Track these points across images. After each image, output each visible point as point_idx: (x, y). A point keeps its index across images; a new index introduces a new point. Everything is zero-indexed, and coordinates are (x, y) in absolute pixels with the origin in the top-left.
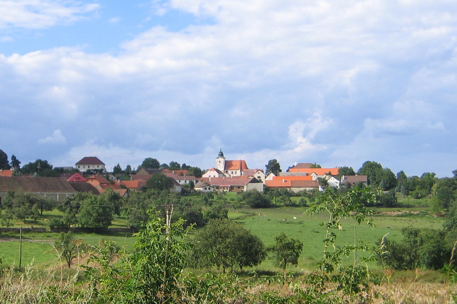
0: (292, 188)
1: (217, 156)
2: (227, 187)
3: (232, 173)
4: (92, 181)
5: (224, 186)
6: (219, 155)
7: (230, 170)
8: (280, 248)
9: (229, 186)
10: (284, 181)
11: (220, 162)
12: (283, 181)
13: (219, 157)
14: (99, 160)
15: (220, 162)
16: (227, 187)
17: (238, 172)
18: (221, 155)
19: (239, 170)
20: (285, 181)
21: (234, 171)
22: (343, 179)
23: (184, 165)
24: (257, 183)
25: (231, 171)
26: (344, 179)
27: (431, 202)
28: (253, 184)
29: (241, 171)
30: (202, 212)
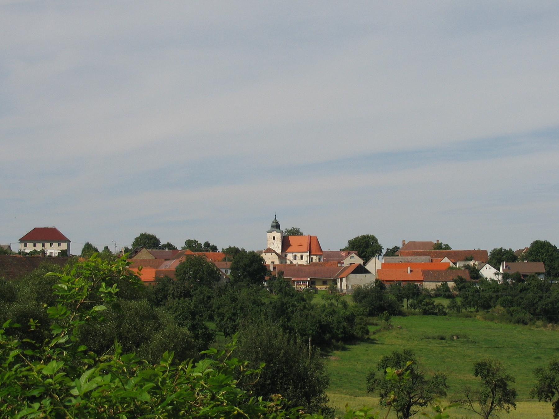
0: (423, 283)
1: (269, 228)
2: (304, 282)
3: (295, 259)
4: (438, 241)
5: (299, 279)
6: (272, 226)
7: (292, 253)
8: (379, 390)
9: (309, 279)
10: (409, 271)
11: (274, 238)
12: (409, 269)
13: (273, 231)
14: (41, 228)
15: (274, 238)
16: (304, 282)
17: (306, 255)
18: (276, 226)
19: (307, 252)
20: (411, 271)
21: (299, 255)
22: (505, 267)
23: (207, 244)
24: (365, 275)
25: (294, 254)
26: (506, 267)
27: (359, 405)
28: (358, 275)
29: (310, 255)
30: (55, 361)
